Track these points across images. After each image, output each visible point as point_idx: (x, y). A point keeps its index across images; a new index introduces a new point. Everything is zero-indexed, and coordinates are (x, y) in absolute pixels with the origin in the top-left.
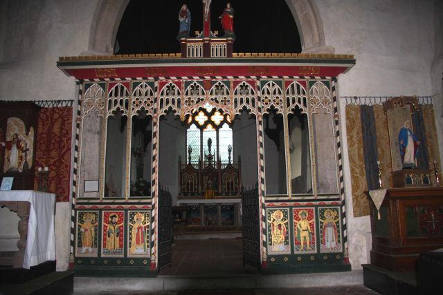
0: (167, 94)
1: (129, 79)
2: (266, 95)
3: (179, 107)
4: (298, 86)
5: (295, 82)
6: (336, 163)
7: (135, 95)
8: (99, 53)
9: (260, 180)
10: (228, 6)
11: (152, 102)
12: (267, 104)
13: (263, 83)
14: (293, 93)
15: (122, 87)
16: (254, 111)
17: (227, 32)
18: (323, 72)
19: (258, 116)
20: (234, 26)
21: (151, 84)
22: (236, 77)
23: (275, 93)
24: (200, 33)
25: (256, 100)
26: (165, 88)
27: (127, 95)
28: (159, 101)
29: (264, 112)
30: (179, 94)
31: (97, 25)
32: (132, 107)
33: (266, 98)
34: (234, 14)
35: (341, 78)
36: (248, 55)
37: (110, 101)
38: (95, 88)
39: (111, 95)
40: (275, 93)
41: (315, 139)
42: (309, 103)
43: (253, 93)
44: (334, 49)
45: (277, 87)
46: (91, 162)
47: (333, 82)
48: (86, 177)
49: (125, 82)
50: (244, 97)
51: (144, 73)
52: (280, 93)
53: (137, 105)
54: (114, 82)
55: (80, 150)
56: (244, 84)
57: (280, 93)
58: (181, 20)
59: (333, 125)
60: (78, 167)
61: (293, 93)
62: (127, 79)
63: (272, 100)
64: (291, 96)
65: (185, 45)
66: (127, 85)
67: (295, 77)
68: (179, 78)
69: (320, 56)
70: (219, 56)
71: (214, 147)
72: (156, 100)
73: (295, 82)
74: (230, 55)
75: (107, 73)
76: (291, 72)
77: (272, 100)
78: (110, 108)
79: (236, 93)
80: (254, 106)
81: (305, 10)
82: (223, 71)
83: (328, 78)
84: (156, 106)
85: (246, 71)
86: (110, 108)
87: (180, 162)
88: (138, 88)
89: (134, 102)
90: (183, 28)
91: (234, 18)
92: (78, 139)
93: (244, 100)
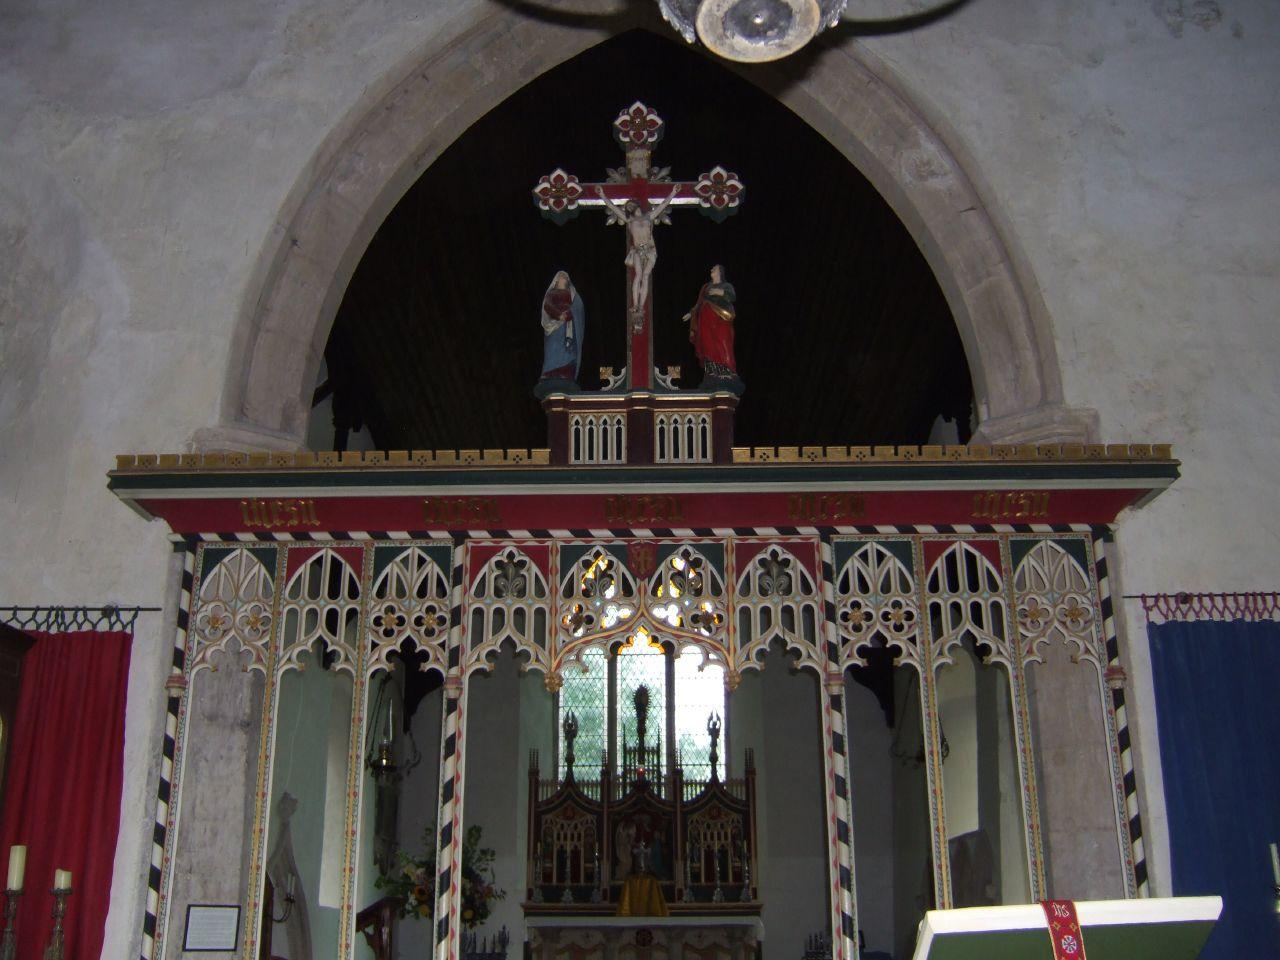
0: (498, 593)
1: (360, 536)
2: (855, 593)
3: (540, 639)
4: (971, 559)
5: (960, 547)
6: (1118, 809)
7: (381, 593)
8: (247, 442)
9: (836, 922)
10: (716, 274)
11: (442, 620)
12: (857, 628)
13: (844, 551)
14: (954, 586)
15: (336, 567)
16: (813, 657)
17: (711, 369)
18: (1061, 510)
19: (830, 676)
20: (738, 350)
21: (442, 556)
22: (744, 531)
23: (886, 588)
24: (616, 373)
25: (819, 616)
26: (489, 570)
27: (354, 593)
28: (468, 620)
29: (850, 659)
30: (540, 592)
31: (254, 336)
32: (371, 637)
33: (856, 605)
34: (738, 306)
35: (1129, 525)
36: (788, 455)
37: (293, 613)
38: (241, 567)
39: (295, 592)
40: (886, 588)
41: (1037, 750)
42: (1012, 627)
43: (806, 589)
44: (1096, 418)
45: (893, 564)
46: (215, 834)
47: (1100, 543)
48: (196, 895)
49: (346, 545)
50: (775, 603)
51: (417, 517)
52: (905, 588)
53: (388, 633)
54: (307, 545)
55: (179, 796)
56: (774, 554)
57: (905, 588)
58: (550, 326)
59: (1106, 704)
60: (166, 860)
61: (954, 586)
62: (353, 535)
63: (877, 615)
64: (944, 599)
65: (565, 417)
66: (355, 556)
67: (958, 528)
68: (540, 533)
69: (1048, 451)
70: (683, 456)
71: (657, 714)
72: (457, 614)
73: (960, 547)
74: (722, 454)
75: (285, 515)
76: (945, 511)
77: (877, 615)
78: (290, 640)
79: (746, 590)
80: (810, 636)
81: (989, 274)
82: (700, 513)
83: (1081, 529)
84: (454, 637)
85: (783, 512)
86: (290, 640)
87: (534, 773)
88: (392, 569)
89: (378, 621)
90: (557, 357)
91: (737, 322)
92: (175, 713)
93: (777, 617)
